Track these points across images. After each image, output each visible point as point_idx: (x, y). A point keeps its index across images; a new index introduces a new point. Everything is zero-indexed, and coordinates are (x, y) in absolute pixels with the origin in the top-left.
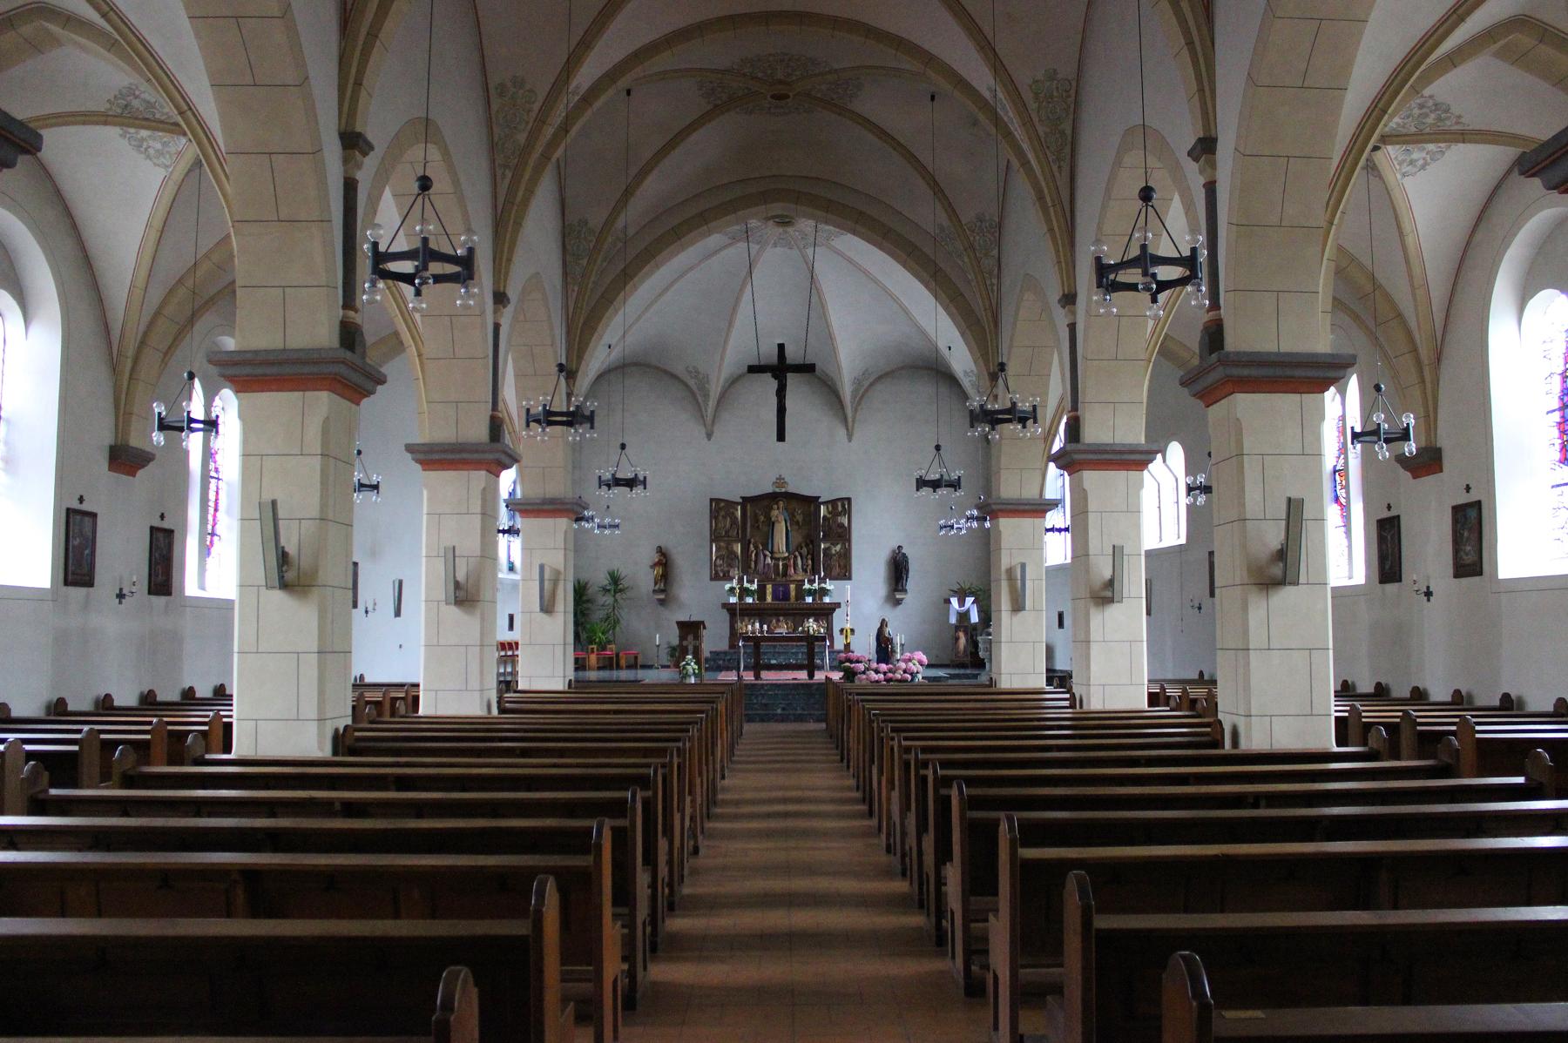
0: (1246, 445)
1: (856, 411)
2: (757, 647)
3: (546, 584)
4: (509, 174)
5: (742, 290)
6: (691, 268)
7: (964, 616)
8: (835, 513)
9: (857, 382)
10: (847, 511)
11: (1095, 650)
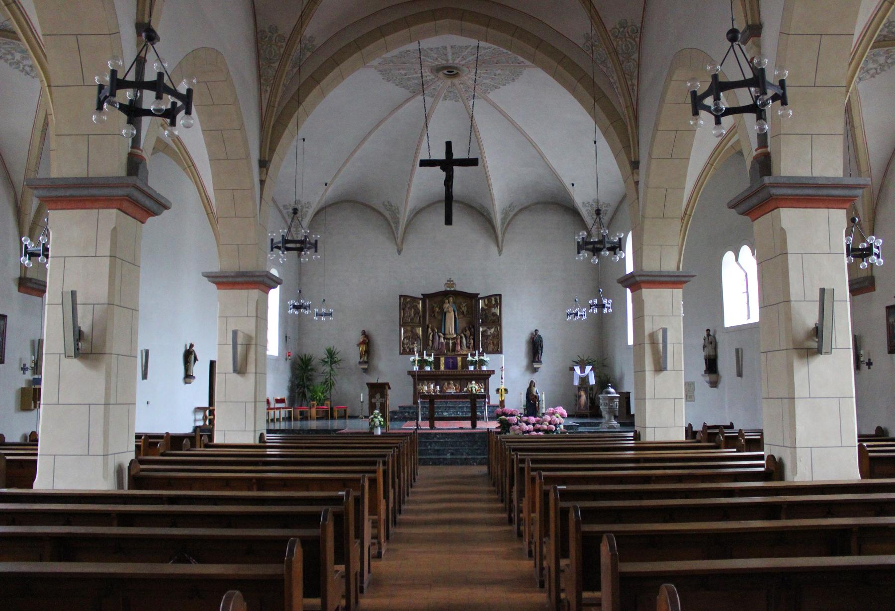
1: (504, 234)
2: (432, 402)
3: (239, 348)
5: (420, 140)
7: (584, 380)
8: (489, 306)
9: (505, 213)
10: (499, 304)
11: (800, 408)
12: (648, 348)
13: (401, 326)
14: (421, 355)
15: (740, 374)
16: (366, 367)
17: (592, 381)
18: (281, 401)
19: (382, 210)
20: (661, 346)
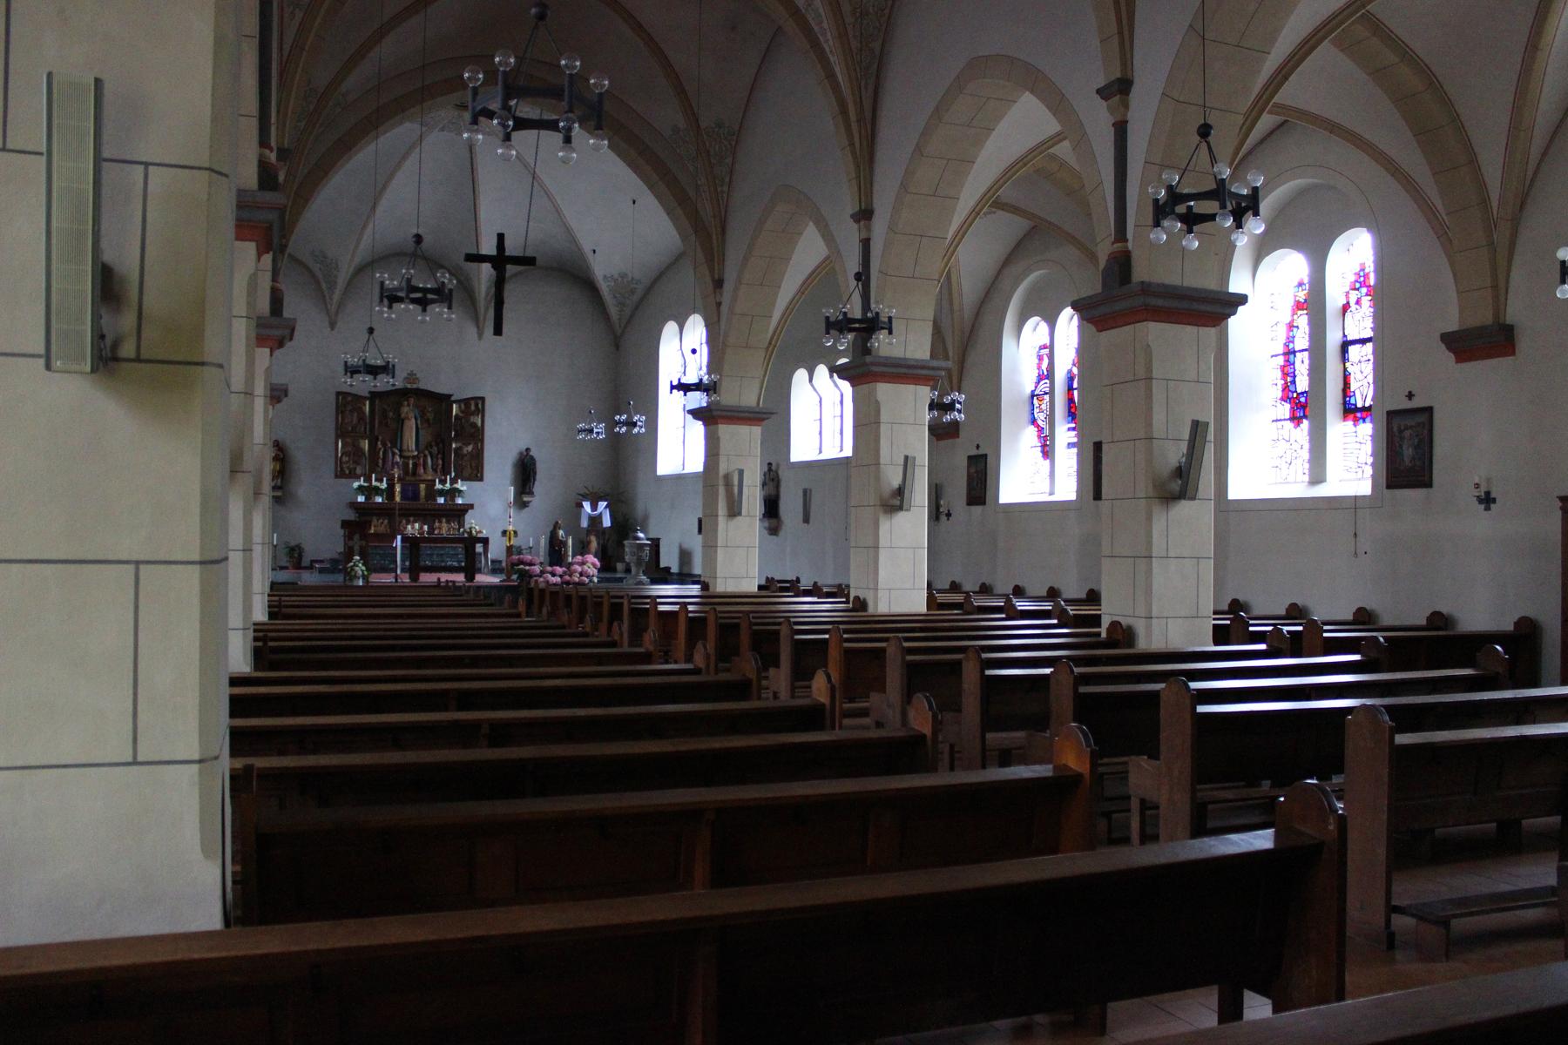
4: (299, 15)
7: (595, 521)
10: (481, 411)
11: (883, 556)
12: (722, 490)
13: (337, 437)
14: (368, 479)
15: (806, 520)
16: (279, 493)
17: (607, 522)
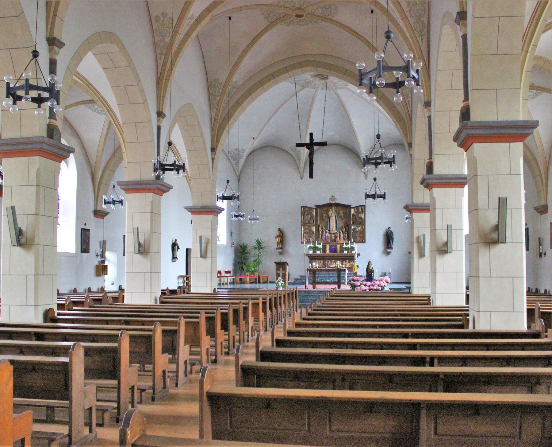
0: (478, 171)
3: (203, 245)
4: (163, 57)
6: (286, 102)
8: (358, 212)
10: (364, 211)
13: (302, 226)
14: (314, 244)
16: (280, 251)
18: (228, 272)
19: (291, 152)
20: (422, 243)
